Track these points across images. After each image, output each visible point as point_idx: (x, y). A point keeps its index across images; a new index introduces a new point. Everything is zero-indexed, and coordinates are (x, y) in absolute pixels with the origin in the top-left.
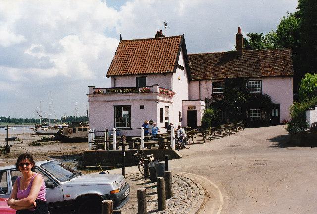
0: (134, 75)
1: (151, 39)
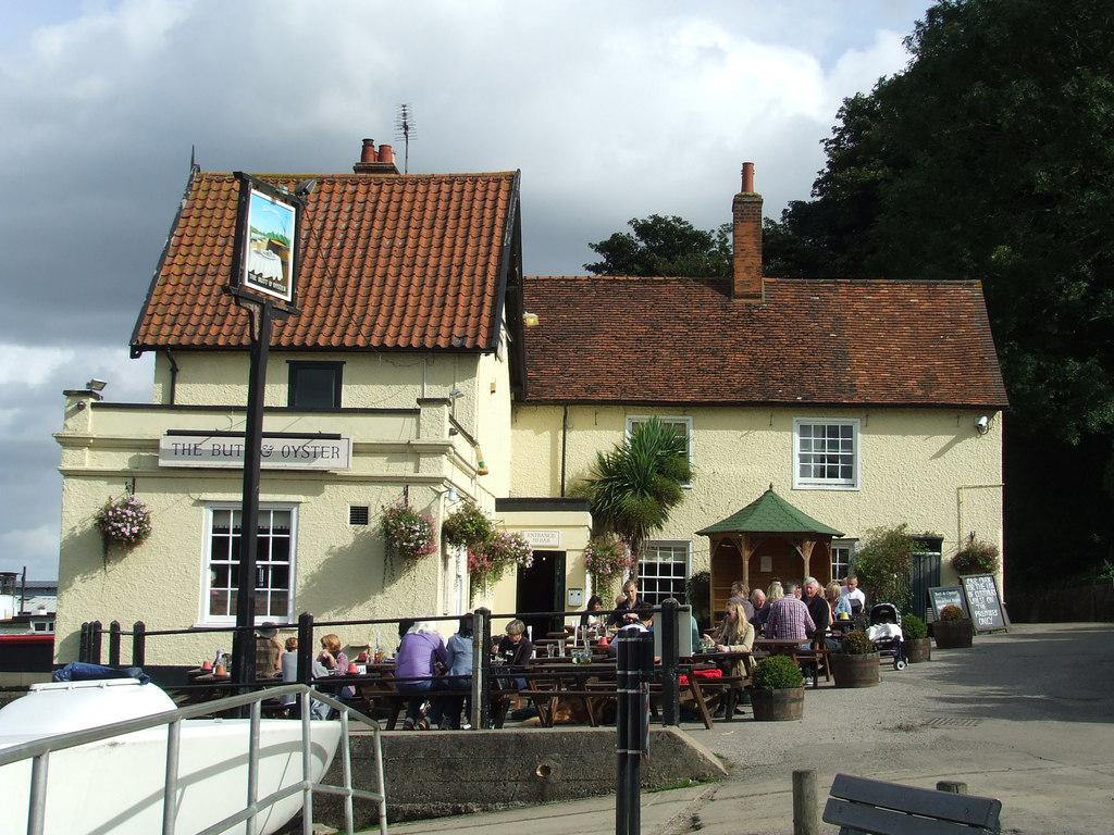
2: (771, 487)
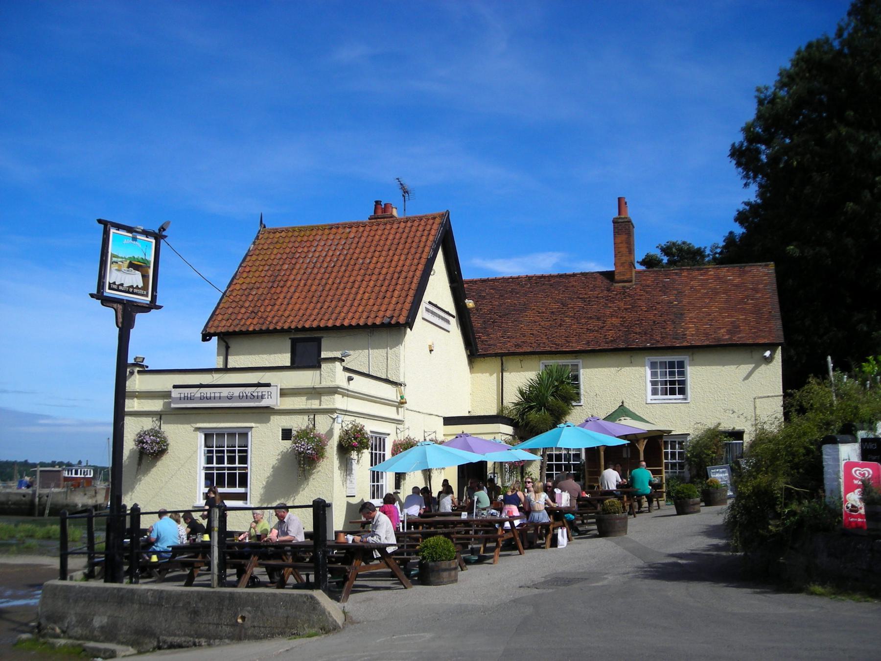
0: (282, 332)
1: (358, 225)
2: (623, 403)
